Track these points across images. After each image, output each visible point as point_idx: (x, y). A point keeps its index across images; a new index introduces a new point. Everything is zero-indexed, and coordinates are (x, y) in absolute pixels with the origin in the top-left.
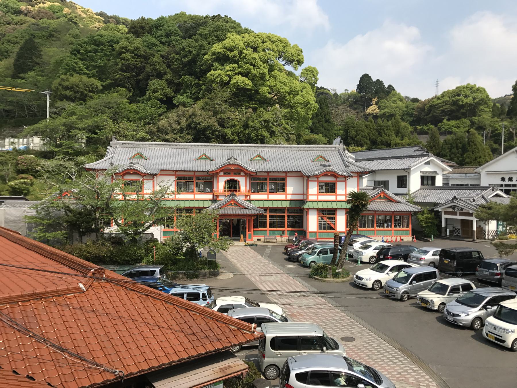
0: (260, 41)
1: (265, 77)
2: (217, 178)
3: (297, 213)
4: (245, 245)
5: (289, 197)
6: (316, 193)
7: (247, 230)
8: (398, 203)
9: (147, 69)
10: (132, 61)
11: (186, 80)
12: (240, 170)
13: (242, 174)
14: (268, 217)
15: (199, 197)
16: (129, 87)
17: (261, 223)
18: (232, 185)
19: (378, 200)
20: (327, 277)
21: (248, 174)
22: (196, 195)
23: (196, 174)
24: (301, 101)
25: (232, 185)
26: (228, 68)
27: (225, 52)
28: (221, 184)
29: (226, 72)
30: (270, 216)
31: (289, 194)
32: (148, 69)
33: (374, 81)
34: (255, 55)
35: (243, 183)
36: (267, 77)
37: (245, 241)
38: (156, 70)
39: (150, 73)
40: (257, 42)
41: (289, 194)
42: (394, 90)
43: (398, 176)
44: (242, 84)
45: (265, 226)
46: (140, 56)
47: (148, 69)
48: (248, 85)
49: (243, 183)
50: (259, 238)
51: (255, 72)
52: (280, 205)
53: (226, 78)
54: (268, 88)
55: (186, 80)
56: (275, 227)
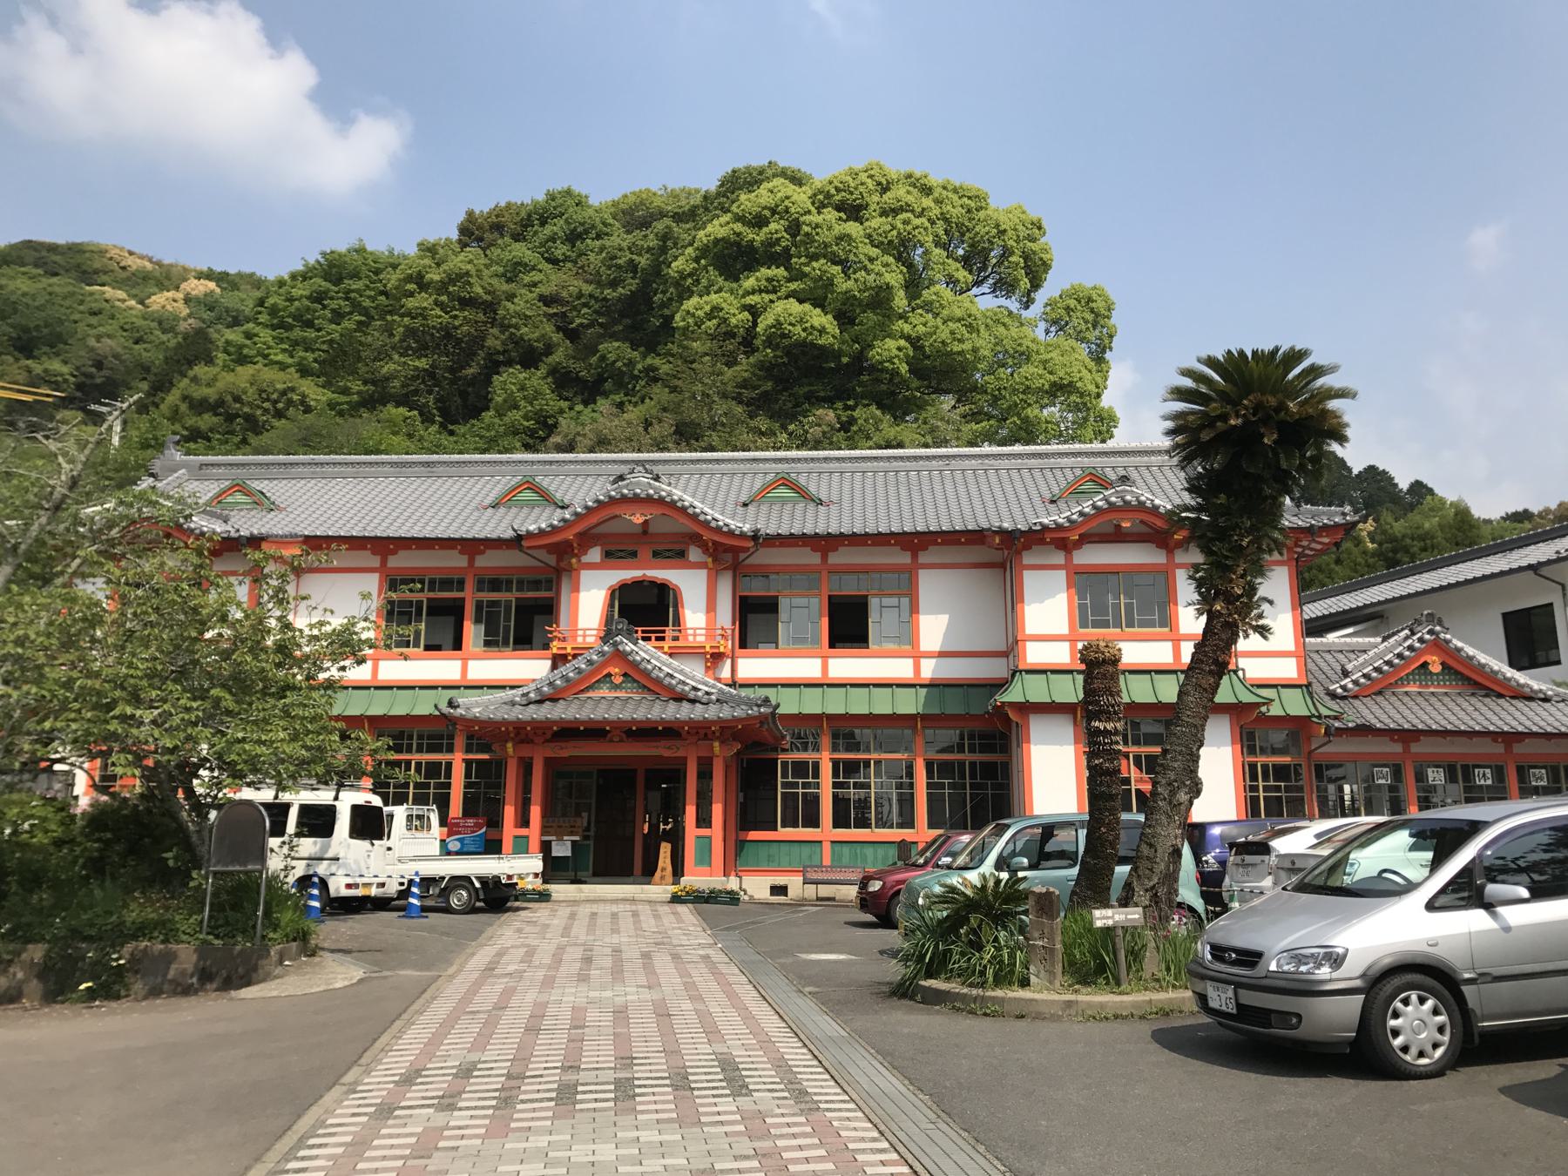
0: (870, 184)
1: (890, 299)
3: (973, 747)
4: (675, 899)
5: (929, 670)
6: (1065, 630)
7: (691, 812)
8: (1530, 699)
9: (489, 342)
10: (438, 317)
11: (611, 357)
12: (685, 537)
13: (694, 554)
14: (826, 769)
15: (495, 677)
16: (426, 405)
17: (790, 799)
18: (645, 609)
19: (1412, 689)
20: (1025, 983)
21: (726, 553)
22: (471, 663)
23: (486, 561)
24: (1038, 383)
25: (645, 609)
26: (750, 283)
27: (738, 234)
28: (588, 605)
29: (743, 296)
30: (836, 763)
31: (929, 655)
32: (495, 339)
33: (1355, 472)
34: (853, 228)
35: (701, 607)
36: (900, 301)
37: (678, 871)
38: (517, 341)
39: (498, 353)
40: (861, 189)
41: (929, 655)
42: (1431, 492)
43: (1505, 616)
44: (798, 329)
45: (813, 821)
46: (468, 303)
47: (495, 339)
48: (822, 331)
49: (701, 607)
50: (780, 880)
51: (850, 284)
52: (882, 704)
53: (740, 318)
54: (902, 343)
55: (611, 357)
56: (863, 823)
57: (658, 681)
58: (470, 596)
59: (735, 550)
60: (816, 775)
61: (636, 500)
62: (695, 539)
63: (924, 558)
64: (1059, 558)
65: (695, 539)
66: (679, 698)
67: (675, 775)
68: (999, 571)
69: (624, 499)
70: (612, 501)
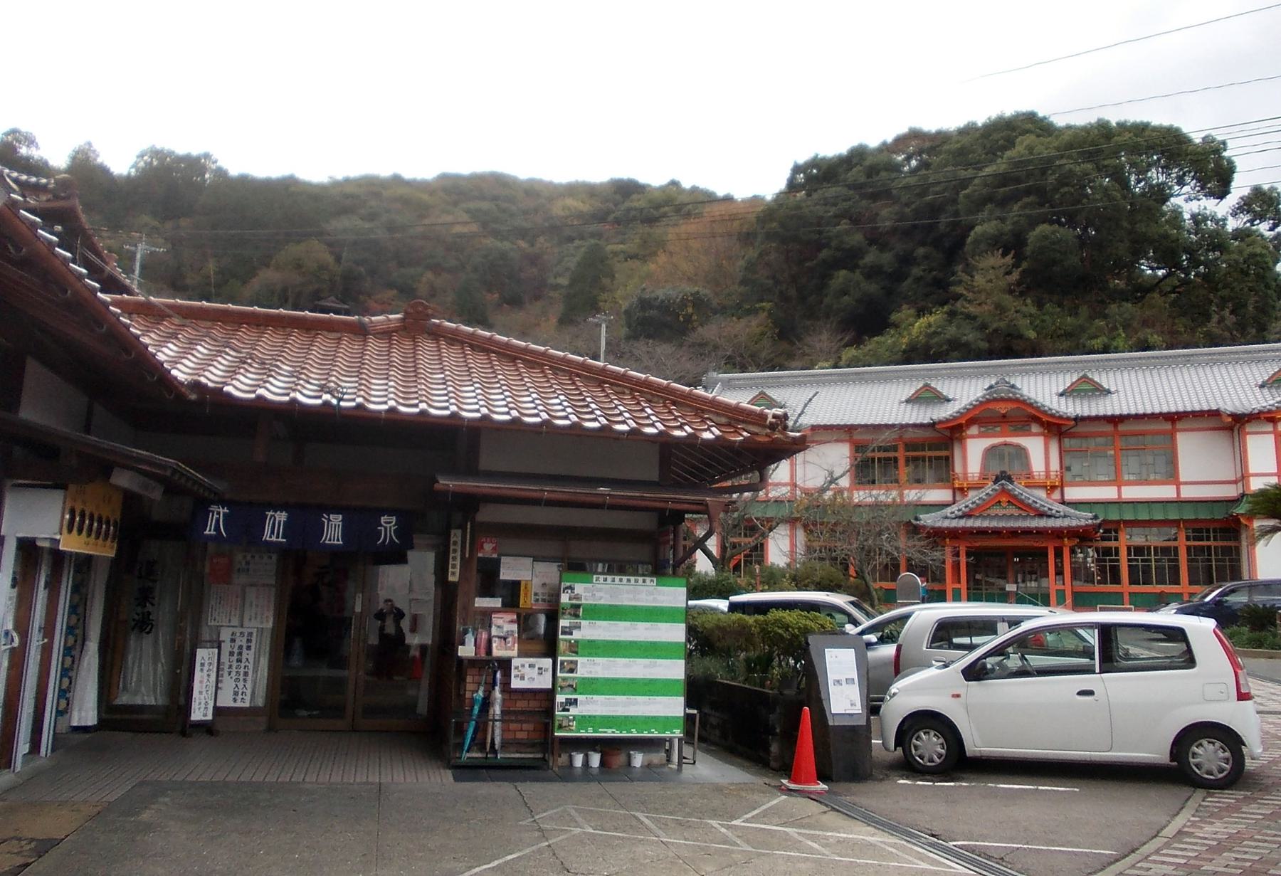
2: (962, 440)
45: (1116, 579)
57: (1029, 506)
58: (901, 454)
59: (1059, 425)
60: (1117, 554)
61: (1002, 400)
62: (1036, 419)
63: (1179, 425)
64: (1270, 427)
65: (1036, 419)
66: (1041, 515)
67: (1043, 553)
68: (1227, 433)
69: (995, 400)
70: (988, 401)
